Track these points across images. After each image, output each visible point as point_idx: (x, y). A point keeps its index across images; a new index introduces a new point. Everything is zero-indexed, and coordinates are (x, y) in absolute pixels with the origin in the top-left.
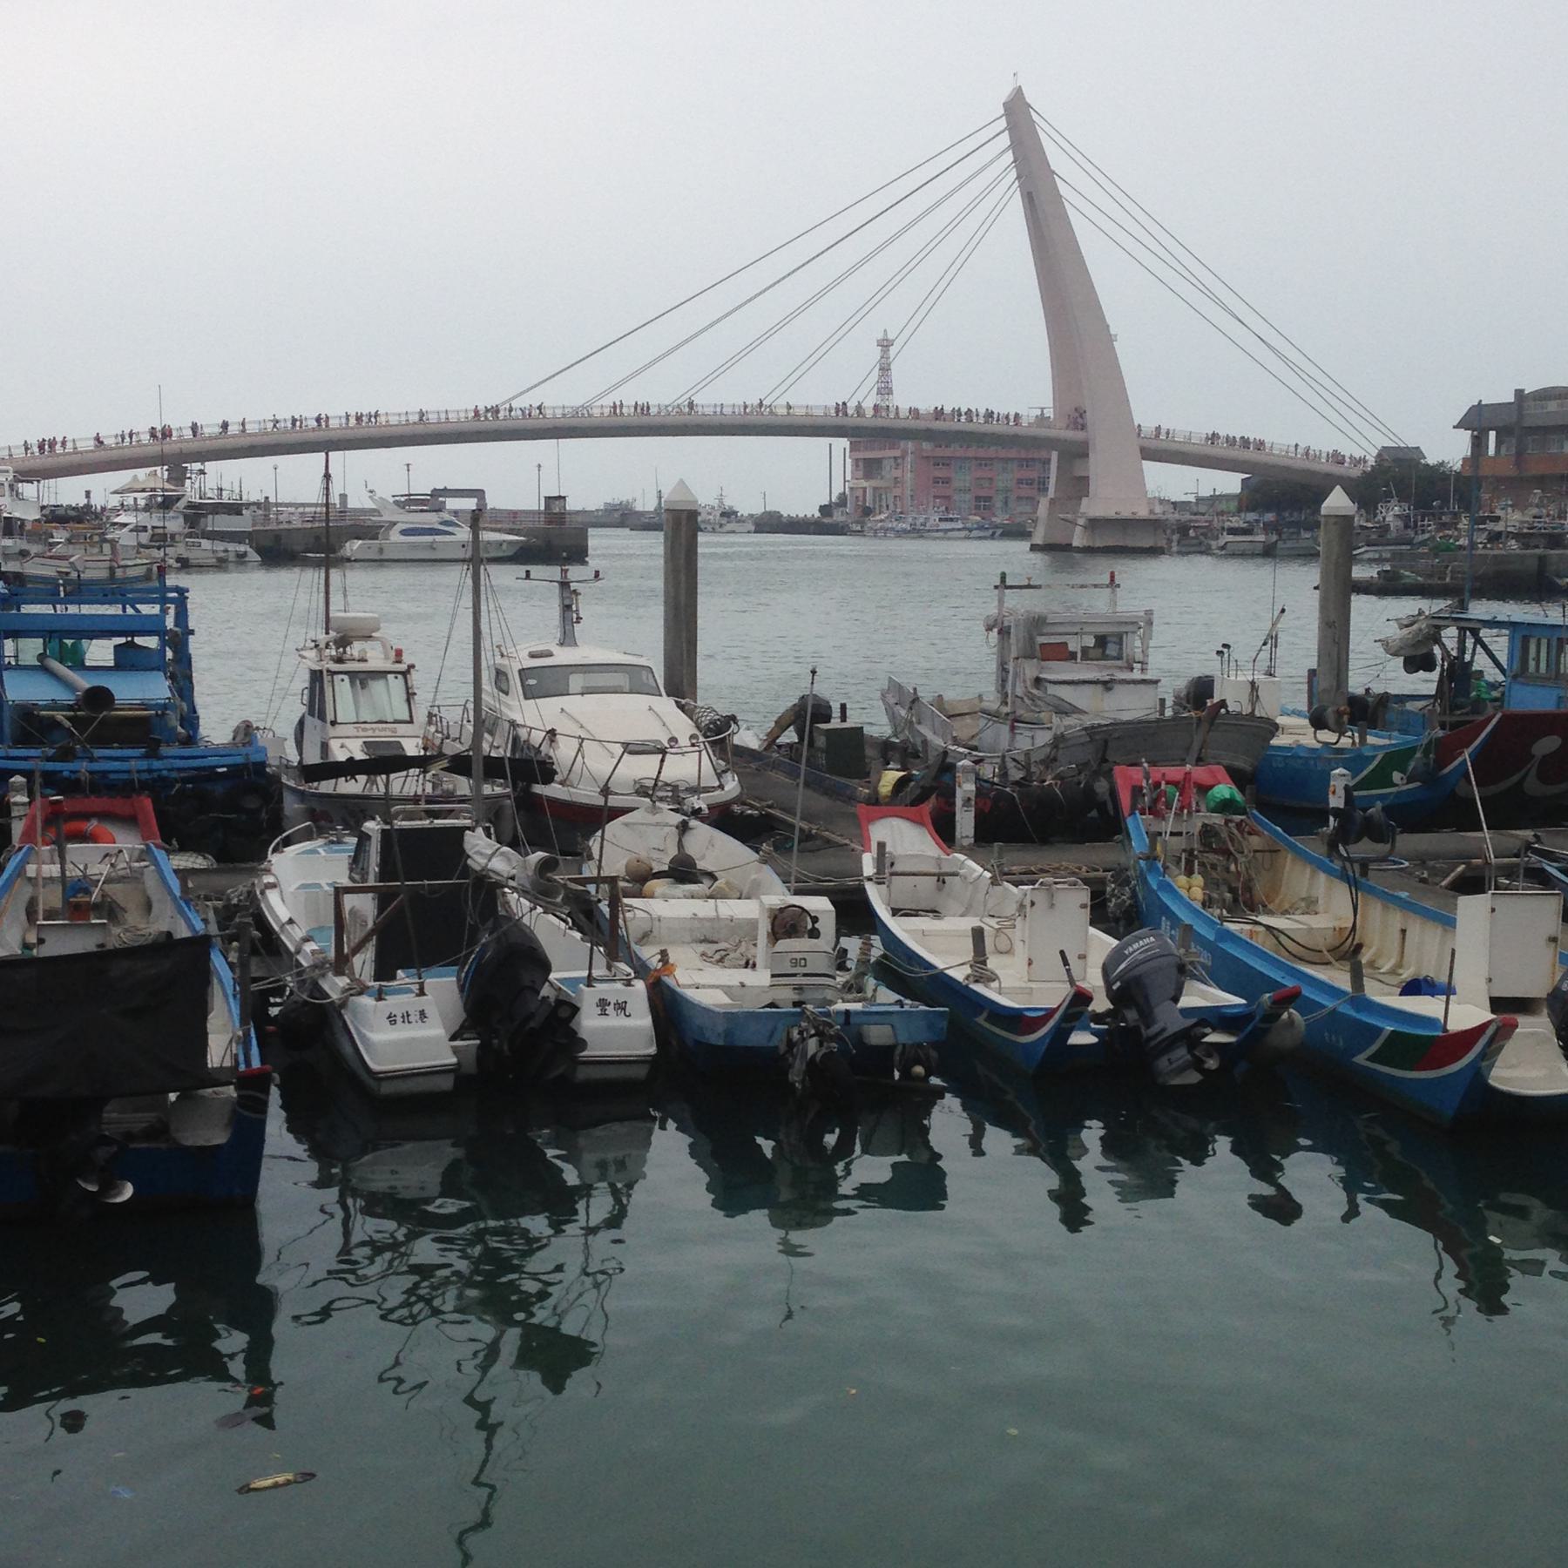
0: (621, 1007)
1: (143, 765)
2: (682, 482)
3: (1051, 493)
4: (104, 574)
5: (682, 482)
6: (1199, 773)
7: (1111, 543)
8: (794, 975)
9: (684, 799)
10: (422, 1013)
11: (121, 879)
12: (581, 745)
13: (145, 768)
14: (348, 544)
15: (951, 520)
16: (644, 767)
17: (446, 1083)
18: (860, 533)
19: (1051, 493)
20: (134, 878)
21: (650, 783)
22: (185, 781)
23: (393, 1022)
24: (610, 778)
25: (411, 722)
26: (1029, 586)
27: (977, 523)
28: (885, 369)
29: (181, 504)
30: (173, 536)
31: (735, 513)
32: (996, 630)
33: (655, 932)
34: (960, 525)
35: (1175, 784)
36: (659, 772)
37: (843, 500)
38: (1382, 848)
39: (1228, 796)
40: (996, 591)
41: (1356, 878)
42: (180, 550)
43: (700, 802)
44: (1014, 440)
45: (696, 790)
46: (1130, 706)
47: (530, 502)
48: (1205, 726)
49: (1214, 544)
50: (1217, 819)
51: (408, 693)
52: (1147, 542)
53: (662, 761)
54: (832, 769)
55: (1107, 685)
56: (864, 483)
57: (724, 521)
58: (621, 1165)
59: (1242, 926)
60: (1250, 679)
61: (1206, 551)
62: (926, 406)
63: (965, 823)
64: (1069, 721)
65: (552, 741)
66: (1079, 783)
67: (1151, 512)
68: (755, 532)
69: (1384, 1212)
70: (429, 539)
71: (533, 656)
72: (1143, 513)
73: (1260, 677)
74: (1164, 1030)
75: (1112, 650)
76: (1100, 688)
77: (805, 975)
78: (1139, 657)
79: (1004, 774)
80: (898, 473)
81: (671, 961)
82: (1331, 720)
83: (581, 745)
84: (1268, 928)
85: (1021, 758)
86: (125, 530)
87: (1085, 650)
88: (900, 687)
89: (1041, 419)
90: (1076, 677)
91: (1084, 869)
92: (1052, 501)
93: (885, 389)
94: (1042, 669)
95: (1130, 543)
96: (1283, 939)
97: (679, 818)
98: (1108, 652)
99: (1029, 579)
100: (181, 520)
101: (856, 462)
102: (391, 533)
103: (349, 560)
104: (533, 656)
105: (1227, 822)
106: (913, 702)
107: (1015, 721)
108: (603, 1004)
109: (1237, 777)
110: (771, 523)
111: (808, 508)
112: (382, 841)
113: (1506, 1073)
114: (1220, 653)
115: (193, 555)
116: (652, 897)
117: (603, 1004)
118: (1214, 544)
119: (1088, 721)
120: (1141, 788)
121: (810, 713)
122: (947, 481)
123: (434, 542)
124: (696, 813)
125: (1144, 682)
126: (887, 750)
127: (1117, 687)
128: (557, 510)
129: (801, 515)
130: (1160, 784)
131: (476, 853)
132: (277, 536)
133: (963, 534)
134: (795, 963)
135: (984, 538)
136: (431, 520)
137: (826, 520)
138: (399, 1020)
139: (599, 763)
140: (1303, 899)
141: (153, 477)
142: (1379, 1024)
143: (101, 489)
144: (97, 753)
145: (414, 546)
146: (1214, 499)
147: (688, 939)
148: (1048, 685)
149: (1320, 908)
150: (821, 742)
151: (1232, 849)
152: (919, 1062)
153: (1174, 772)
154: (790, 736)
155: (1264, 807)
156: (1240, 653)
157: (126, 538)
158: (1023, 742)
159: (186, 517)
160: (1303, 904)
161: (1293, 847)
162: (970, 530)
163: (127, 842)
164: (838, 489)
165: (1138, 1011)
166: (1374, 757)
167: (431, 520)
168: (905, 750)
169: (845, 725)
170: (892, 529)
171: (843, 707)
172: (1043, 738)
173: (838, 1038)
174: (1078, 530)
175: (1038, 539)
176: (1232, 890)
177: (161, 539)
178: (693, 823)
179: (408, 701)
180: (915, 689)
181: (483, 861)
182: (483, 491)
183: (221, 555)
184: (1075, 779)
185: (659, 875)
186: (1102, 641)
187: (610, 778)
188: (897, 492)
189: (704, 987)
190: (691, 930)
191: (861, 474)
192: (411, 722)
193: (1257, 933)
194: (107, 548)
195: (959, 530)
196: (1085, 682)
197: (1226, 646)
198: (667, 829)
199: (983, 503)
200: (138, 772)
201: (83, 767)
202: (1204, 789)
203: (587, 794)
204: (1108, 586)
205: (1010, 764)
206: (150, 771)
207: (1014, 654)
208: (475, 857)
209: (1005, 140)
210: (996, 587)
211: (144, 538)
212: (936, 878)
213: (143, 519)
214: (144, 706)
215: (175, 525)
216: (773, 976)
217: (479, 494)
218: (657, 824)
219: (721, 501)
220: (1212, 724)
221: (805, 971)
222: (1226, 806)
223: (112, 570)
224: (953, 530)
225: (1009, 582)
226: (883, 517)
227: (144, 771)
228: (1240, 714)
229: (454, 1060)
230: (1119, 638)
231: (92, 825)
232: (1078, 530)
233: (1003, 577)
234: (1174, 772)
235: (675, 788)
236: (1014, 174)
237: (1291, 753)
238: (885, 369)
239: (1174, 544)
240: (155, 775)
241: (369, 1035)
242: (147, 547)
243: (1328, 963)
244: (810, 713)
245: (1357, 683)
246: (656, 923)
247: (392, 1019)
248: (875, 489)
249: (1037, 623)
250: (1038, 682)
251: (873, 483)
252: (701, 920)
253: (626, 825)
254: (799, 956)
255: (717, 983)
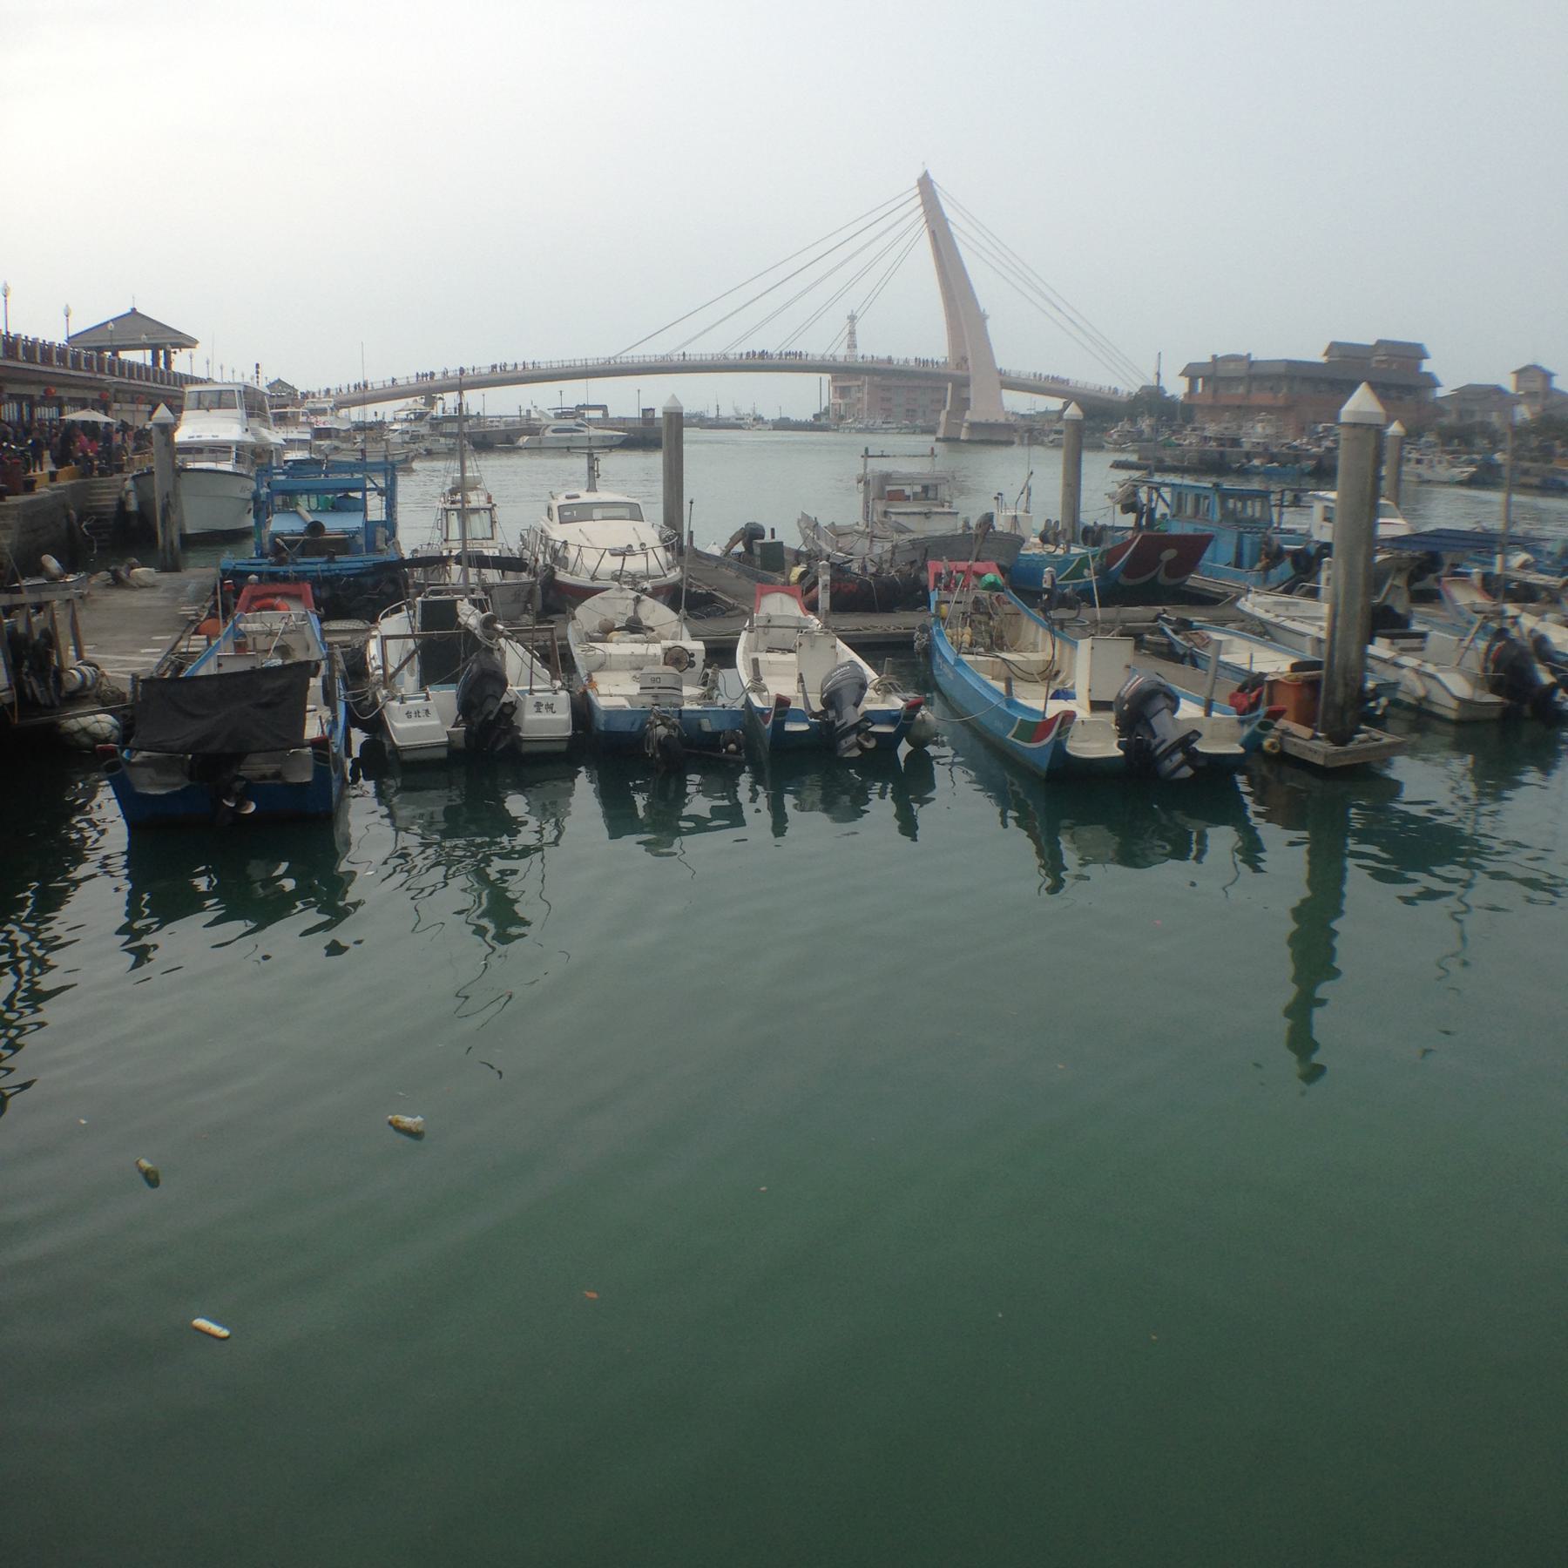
0: (550, 707)
1: (325, 567)
2: (673, 396)
3: (948, 408)
4: (382, 459)
5: (673, 396)
6: (978, 566)
7: (983, 438)
8: (652, 688)
9: (639, 583)
10: (427, 711)
11: (291, 632)
12: (580, 550)
13: (326, 568)
14: (521, 439)
15: (889, 423)
16: (612, 564)
17: (443, 753)
18: (837, 430)
19: (948, 408)
20: (298, 630)
21: (618, 573)
22: (349, 576)
23: (410, 717)
24: (596, 570)
25: (492, 539)
26: (882, 456)
27: (906, 424)
28: (852, 333)
29: (428, 417)
30: (423, 436)
31: (763, 418)
32: (863, 483)
33: (608, 663)
34: (894, 426)
35: (962, 572)
36: (623, 566)
37: (827, 411)
38: (1073, 613)
39: (992, 580)
40: (863, 459)
41: (1057, 628)
42: (427, 444)
43: (647, 585)
44: (927, 376)
45: (647, 577)
46: (939, 527)
47: (634, 413)
48: (980, 539)
49: (1046, 440)
50: (985, 594)
51: (492, 522)
52: (1004, 438)
53: (624, 559)
54: (765, 567)
55: (927, 515)
56: (840, 401)
57: (755, 423)
58: (554, 803)
59: (988, 658)
60: (1014, 514)
61: (1042, 444)
62: (882, 354)
63: (824, 600)
64: (903, 537)
65: (566, 548)
66: (911, 575)
67: (1007, 419)
68: (774, 429)
69: (1223, 827)
70: (569, 435)
71: (568, 498)
72: (1002, 420)
73: (1020, 513)
74: (845, 723)
75: (931, 494)
76: (923, 517)
77: (659, 688)
78: (948, 498)
79: (864, 568)
80: (860, 395)
81: (594, 680)
82: (1051, 538)
83: (580, 550)
84: (1004, 660)
85: (877, 560)
86: (397, 433)
87: (915, 494)
88: (808, 517)
89: (945, 363)
90: (909, 510)
91: (892, 627)
92: (948, 413)
93: (852, 345)
94: (889, 506)
95: (995, 438)
96: (1012, 666)
97: (634, 594)
98: (929, 496)
99: (882, 451)
100: (428, 427)
101: (835, 388)
102: (546, 431)
103: (520, 448)
104: (568, 498)
105: (990, 596)
106: (814, 526)
107: (872, 537)
108: (538, 705)
109: (1003, 570)
110: (783, 425)
111: (806, 416)
112: (422, 609)
113: (1078, 745)
114: (996, 498)
115: (435, 447)
116: (611, 642)
117: (538, 705)
118: (1046, 440)
119: (915, 536)
120: (941, 574)
121: (751, 534)
122: (889, 400)
123: (572, 436)
124: (644, 591)
125: (949, 513)
126: (798, 556)
127: (933, 517)
128: (650, 417)
129: (804, 420)
130: (952, 572)
131: (463, 614)
132: (484, 435)
133: (897, 431)
134: (654, 680)
135: (909, 433)
136: (570, 423)
137: (818, 423)
138: (413, 715)
139: (590, 560)
140: (1031, 644)
141: (416, 403)
142: (1016, 716)
143: (386, 411)
144: (300, 560)
145: (558, 439)
146: (1047, 412)
147: (628, 667)
148: (892, 515)
149: (1040, 648)
150: (757, 551)
151: (992, 612)
152: (732, 742)
153: (962, 565)
154: (740, 548)
155: (1017, 591)
156: (1009, 498)
157: (395, 438)
158: (877, 549)
159: (432, 425)
160: (1031, 646)
161: (1030, 614)
162: (901, 429)
163: (295, 610)
164: (825, 404)
165: (836, 712)
166: (1074, 560)
167: (570, 423)
168: (810, 555)
169: (774, 541)
170: (854, 428)
171: (773, 530)
172: (888, 546)
173: (674, 727)
174: (964, 430)
175: (940, 435)
176: (991, 637)
177: (416, 438)
178: (644, 597)
179: (492, 526)
180: (816, 518)
181: (465, 619)
182: (606, 406)
183: (451, 446)
184: (909, 572)
185: (618, 629)
186: (926, 489)
187: (596, 570)
188: (859, 406)
189: (615, 695)
190: (630, 662)
191: (838, 395)
192: (492, 539)
193: (997, 663)
194: (384, 443)
195: (893, 428)
196: (914, 513)
197: (999, 494)
198: (628, 601)
199: (911, 413)
200: (322, 571)
201: (291, 568)
202: (979, 575)
203: (583, 580)
204: (929, 456)
205: (869, 564)
206: (329, 570)
207: (871, 498)
208: (463, 616)
209: (918, 200)
210: (862, 456)
211: (407, 437)
212: (796, 630)
213: (405, 426)
214: (345, 533)
215: (424, 429)
216: (641, 688)
217: (603, 408)
218: (622, 598)
219: (754, 413)
220: (984, 538)
221: (661, 685)
222: (992, 586)
223: (386, 457)
224: (890, 428)
225: (870, 454)
226: (850, 421)
227: (326, 571)
228: (1002, 532)
229: (446, 739)
230: (936, 486)
231: (277, 601)
232: (964, 430)
233: (867, 450)
234: (962, 565)
235: (633, 576)
236: (924, 220)
237: (1031, 558)
238: (852, 333)
239: (1026, 439)
240: (333, 573)
241: (395, 724)
242: (407, 443)
243: (1037, 682)
244: (751, 534)
245: (1088, 518)
246: (608, 658)
247: (408, 714)
248: (846, 404)
249: (886, 478)
250: (886, 513)
251: (847, 401)
252: (635, 656)
253: (603, 598)
254: (656, 676)
255: (623, 693)
